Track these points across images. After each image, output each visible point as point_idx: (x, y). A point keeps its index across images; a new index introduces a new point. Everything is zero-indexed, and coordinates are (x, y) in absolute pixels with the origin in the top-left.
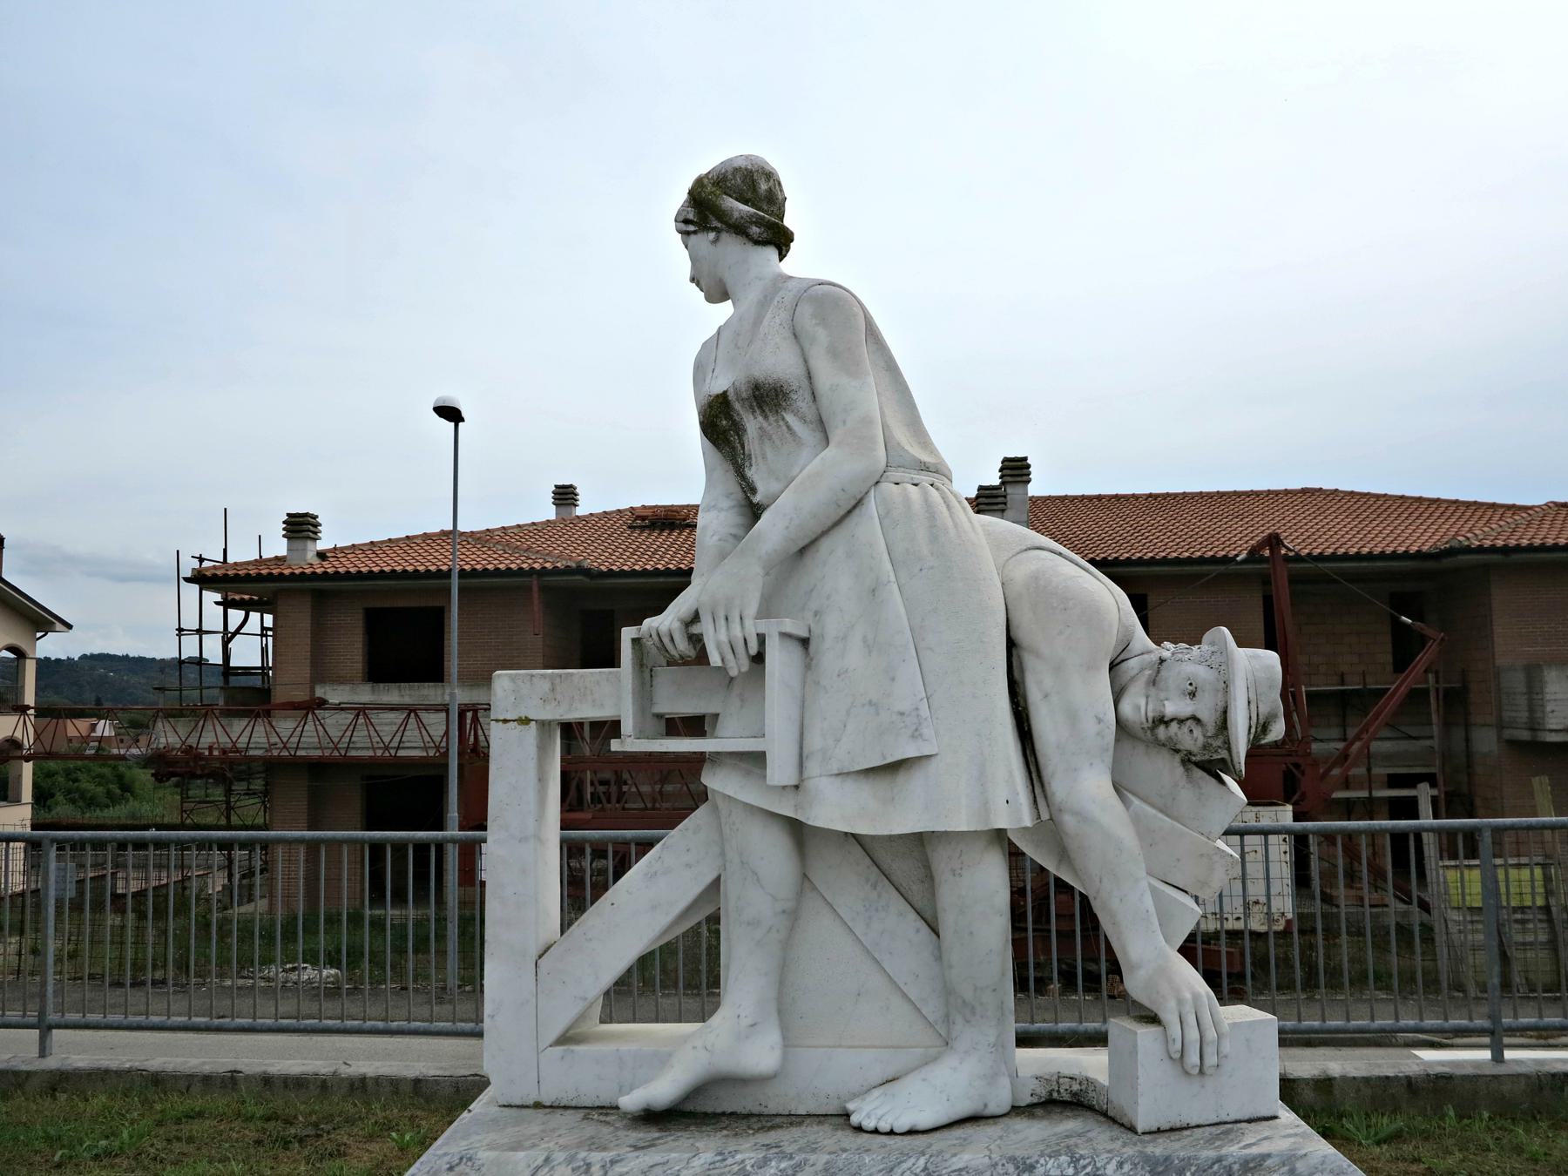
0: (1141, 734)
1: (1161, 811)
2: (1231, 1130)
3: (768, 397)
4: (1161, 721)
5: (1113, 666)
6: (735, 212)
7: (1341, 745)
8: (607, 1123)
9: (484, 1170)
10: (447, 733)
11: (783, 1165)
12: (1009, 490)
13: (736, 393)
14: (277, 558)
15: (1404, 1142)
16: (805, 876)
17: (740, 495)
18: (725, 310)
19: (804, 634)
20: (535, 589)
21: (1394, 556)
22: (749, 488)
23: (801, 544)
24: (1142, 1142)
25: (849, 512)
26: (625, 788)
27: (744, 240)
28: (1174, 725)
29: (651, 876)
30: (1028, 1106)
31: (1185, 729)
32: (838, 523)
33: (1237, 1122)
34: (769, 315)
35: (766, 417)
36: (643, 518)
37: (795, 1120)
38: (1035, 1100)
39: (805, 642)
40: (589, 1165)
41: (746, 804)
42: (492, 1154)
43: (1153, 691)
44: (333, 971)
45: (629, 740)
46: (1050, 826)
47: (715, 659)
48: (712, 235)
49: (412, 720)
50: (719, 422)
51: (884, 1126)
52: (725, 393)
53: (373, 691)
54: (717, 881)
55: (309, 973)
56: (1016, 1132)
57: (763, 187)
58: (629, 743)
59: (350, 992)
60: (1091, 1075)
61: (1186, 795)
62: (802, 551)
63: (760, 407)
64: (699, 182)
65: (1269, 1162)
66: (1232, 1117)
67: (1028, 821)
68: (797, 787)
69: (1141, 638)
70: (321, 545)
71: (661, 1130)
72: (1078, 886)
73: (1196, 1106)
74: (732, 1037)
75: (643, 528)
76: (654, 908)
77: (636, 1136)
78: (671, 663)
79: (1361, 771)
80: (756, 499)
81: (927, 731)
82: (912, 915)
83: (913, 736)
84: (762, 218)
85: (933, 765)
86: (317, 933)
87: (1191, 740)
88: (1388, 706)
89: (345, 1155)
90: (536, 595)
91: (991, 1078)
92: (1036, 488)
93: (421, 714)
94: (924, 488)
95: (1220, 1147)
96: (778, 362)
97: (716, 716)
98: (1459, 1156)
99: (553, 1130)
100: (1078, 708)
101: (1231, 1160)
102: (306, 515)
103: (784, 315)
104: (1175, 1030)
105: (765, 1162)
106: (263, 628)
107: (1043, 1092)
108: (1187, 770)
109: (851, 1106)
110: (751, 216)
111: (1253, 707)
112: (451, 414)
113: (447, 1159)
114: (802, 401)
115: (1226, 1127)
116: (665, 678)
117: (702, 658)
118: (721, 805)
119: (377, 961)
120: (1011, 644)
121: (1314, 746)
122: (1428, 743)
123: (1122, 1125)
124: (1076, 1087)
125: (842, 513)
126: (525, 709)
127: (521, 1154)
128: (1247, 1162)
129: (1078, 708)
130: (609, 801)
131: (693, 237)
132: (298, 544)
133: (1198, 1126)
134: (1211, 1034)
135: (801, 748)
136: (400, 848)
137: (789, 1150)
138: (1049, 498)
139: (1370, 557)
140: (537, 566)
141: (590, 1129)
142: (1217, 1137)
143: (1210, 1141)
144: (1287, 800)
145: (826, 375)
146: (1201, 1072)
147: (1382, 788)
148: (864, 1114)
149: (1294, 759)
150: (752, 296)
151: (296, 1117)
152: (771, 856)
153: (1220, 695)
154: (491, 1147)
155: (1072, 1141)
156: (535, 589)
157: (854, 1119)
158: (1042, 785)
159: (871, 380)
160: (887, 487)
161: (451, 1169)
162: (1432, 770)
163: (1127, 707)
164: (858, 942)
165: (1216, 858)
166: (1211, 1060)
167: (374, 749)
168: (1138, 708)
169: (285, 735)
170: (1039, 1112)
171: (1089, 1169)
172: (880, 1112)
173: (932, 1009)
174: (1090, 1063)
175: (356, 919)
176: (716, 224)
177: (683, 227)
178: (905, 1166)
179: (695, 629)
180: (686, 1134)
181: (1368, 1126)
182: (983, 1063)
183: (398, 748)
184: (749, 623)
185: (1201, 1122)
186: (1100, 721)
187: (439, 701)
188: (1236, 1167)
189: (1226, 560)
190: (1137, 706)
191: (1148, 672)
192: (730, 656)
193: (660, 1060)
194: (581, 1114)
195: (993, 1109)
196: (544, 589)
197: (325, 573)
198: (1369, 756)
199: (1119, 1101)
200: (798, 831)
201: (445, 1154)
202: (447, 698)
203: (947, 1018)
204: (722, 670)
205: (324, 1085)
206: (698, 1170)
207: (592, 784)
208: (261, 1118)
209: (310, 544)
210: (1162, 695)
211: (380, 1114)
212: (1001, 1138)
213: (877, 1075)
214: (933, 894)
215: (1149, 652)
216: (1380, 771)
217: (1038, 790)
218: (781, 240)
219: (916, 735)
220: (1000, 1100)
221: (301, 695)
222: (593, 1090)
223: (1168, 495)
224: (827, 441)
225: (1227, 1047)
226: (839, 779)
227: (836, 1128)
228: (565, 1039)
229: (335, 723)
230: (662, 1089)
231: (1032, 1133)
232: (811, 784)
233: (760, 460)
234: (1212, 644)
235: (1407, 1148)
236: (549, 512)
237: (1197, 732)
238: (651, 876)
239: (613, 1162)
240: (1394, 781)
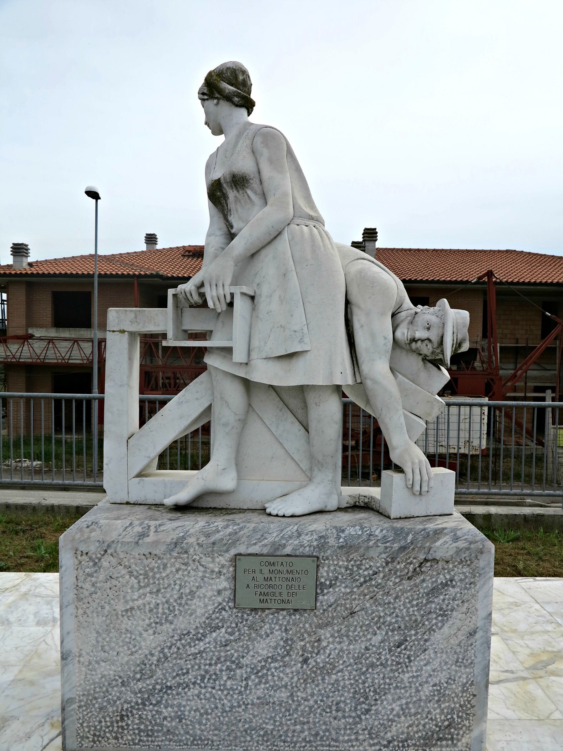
0: (404, 346)
1: (412, 381)
2: (432, 519)
3: (239, 181)
4: (414, 340)
5: (393, 315)
6: (227, 89)
7: (512, 372)
8: (159, 510)
9: (102, 527)
10: (92, 352)
11: (235, 528)
12: (367, 244)
13: (224, 179)
14: (8, 265)
15: (520, 541)
16: (250, 405)
17: (226, 229)
18: (221, 138)
19: (252, 294)
20: (136, 285)
21: (546, 284)
22: (230, 226)
23: (252, 252)
24: (392, 522)
25: (275, 238)
26: (178, 381)
27: (231, 104)
28: (419, 342)
29: (180, 403)
30: (345, 508)
31: (424, 344)
32: (269, 243)
33: (434, 516)
34: (241, 142)
35: (238, 191)
36: (189, 252)
37: (242, 511)
38: (348, 505)
39: (253, 298)
40: (149, 526)
41: (224, 371)
42: (107, 521)
43: (411, 326)
44: (39, 462)
45: (171, 341)
46: (360, 384)
47: (210, 304)
48: (215, 101)
49: (76, 343)
50: (217, 194)
51: (281, 514)
52: (219, 179)
53: (57, 332)
54: (210, 406)
55: (27, 463)
56: (338, 517)
57: (241, 78)
58: (171, 342)
59: (46, 472)
60: (373, 495)
61: (423, 375)
62: (253, 255)
63: (235, 186)
64: (210, 74)
65: (445, 531)
66: (433, 514)
67: (350, 382)
68: (247, 364)
69: (408, 302)
70: (30, 260)
71: (182, 513)
72: (373, 415)
73: (418, 508)
74: (215, 475)
75: (189, 256)
76: (181, 418)
77: (170, 515)
78: (191, 306)
79: (522, 384)
80: (233, 231)
81: (306, 340)
82: (297, 424)
83: (300, 342)
84: (240, 93)
85: (308, 356)
86: (30, 445)
87: (426, 349)
88: (535, 355)
89: (44, 537)
90: (136, 288)
91: (329, 495)
92: (380, 244)
93: (81, 343)
94: (310, 228)
95: (426, 525)
96: (244, 164)
97: (211, 331)
98: (542, 547)
99: (134, 513)
100: (375, 333)
101: (429, 529)
102: (22, 244)
103: (248, 142)
104: (410, 475)
105: (227, 527)
106: (2, 300)
107: (352, 502)
108: (424, 363)
109: (266, 505)
110: (235, 92)
111: (455, 335)
112: (93, 195)
113: (86, 523)
114: (255, 183)
115: (429, 517)
116: (188, 313)
117: (204, 304)
118: (212, 371)
119: (58, 457)
120: (347, 303)
121: (501, 372)
122: (553, 372)
123: (385, 516)
124: (366, 500)
125: (272, 237)
126: (123, 327)
127: (119, 521)
128: (436, 531)
129: (375, 333)
130: (170, 387)
131: (206, 102)
132: (19, 259)
133: (417, 517)
134: (425, 478)
135: (249, 346)
136: (69, 401)
137: (238, 522)
138: (386, 249)
139: (535, 284)
140: (136, 273)
141: (150, 513)
142: (425, 521)
143: (421, 523)
144: (486, 396)
145: (267, 172)
146: (420, 494)
147: (531, 392)
148: (272, 508)
149: (491, 377)
150: (233, 132)
151: (21, 522)
152: (234, 394)
153: (441, 329)
154: (106, 518)
155: (362, 521)
156: (136, 285)
157: (268, 511)
158: (358, 367)
159: (288, 175)
160: (293, 226)
161: (88, 527)
162: (555, 385)
163: (398, 334)
164: (273, 435)
165: (435, 403)
166: (425, 489)
167: (57, 359)
168: (404, 334)
169: (14, 351)
170: (350, 510)
171: (368, 532)
172: (279, 508)
173: (304, 465)
174: (374, 492)
175: (48, 439)
176: (217, 95)
177: (201, 96)
178: (288, 529)
179: (202, 290)
180: (193, 515)
181: (505, 535)
182: (328, 488)
183: (69, 359)
184: (226, 287)
185: (419, 515)
186: (385, 338)
187: (89, 336)
188: (431, 533)
189: (467, 282)
190: (403, 333)
191: (409, 318)
192: (217, 303)
193: (183, 484)
194: (147, 507)
195: (329, 508)
196: (140, 284)
197: (32, 273)
198: (526, 377)
199: (384, 506)
200: (247, 384)
201: (86, 521)
202: (93, 336)
203: (311, 469)
204: (214, 310)
205: (34, 509)
206: (198, 529)
207: (162, 378)
208: (5, 522)
209: (24, 259)
210: (415, 328)
211: (61, 521)
212: (331, 519)
213: (279, 492)
214: (307, 415)
215: (411, 309)
216: (530, 384)
217: (356, 369)
218: (249, 105)
219: (301, 341)
220: (333, 504)
221: (21, 332)
222: (152, 498)
223: (443, 250)
224: (266, 203)
225: (432, 484)
226: (265, 361)
227: (260, 514)
228: (140, 475)
229: (39, 346)
230: (183, 496)
231: (344, 518)
232: (253, 363)
233: (235, 212)
234: (440, 306)
235: (521, 544)
236: (142, 247)
237: (430, 346)
238: (180, 403)
239: (160, 525)
240: (537, 389)
